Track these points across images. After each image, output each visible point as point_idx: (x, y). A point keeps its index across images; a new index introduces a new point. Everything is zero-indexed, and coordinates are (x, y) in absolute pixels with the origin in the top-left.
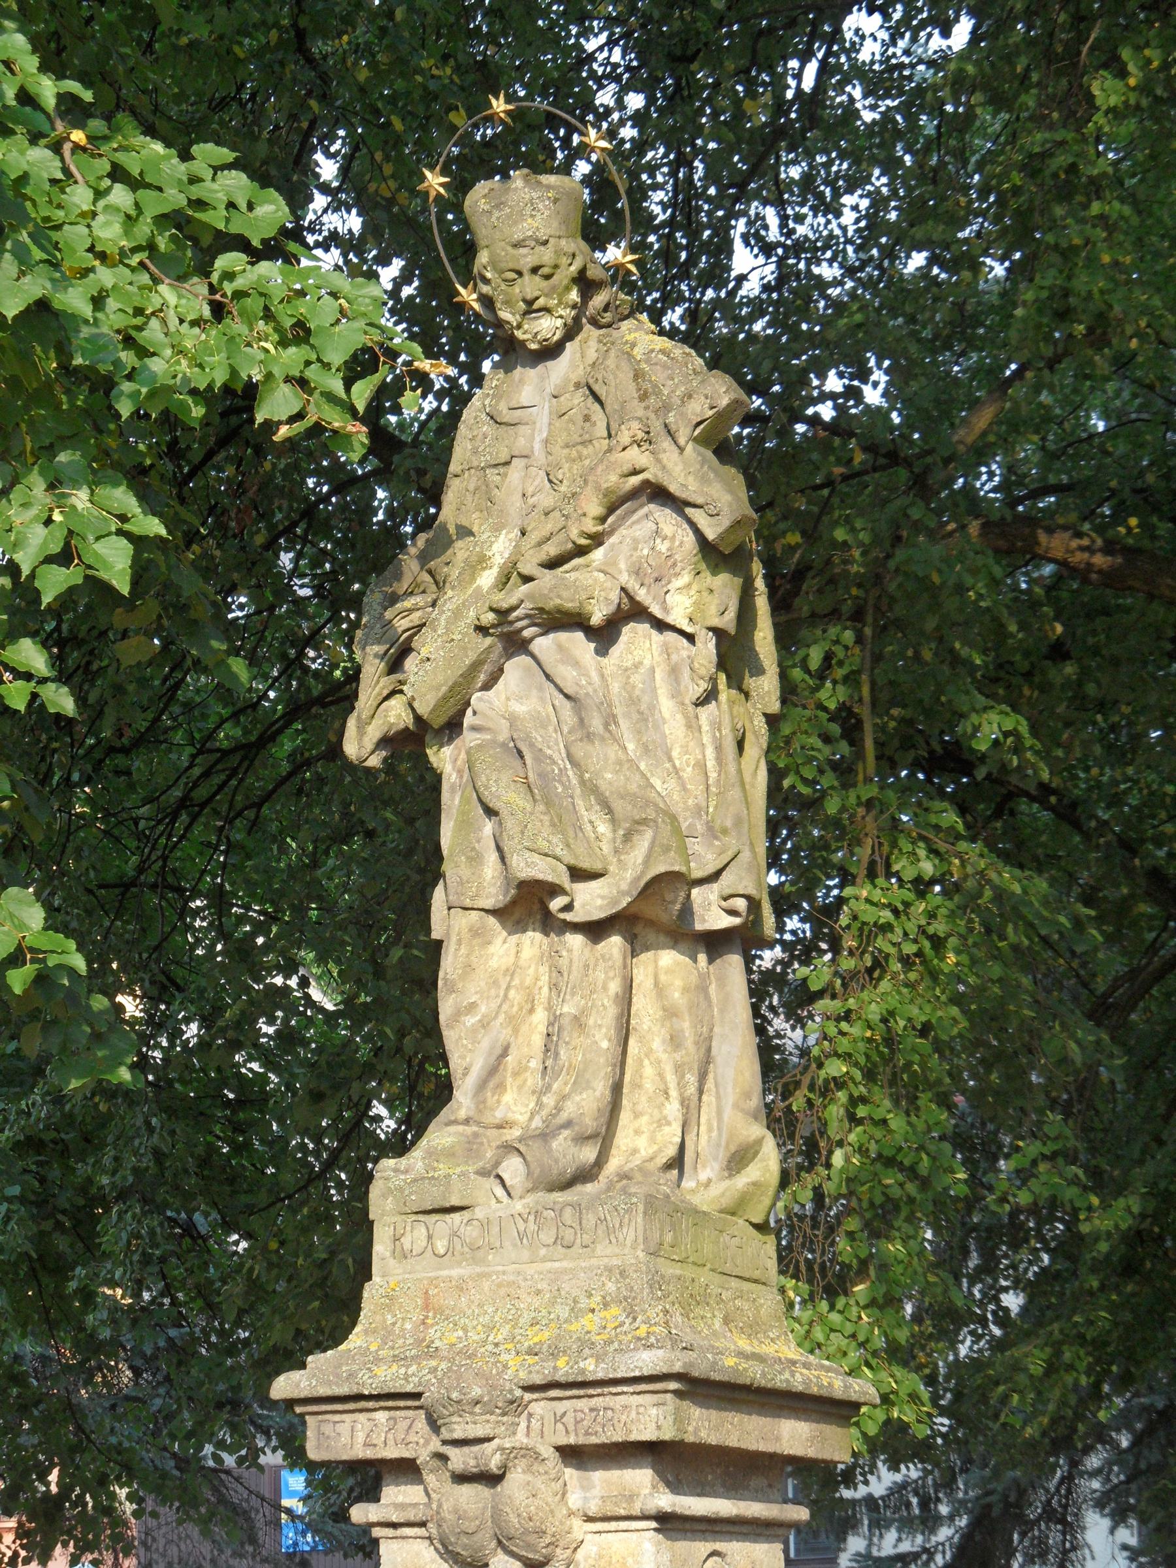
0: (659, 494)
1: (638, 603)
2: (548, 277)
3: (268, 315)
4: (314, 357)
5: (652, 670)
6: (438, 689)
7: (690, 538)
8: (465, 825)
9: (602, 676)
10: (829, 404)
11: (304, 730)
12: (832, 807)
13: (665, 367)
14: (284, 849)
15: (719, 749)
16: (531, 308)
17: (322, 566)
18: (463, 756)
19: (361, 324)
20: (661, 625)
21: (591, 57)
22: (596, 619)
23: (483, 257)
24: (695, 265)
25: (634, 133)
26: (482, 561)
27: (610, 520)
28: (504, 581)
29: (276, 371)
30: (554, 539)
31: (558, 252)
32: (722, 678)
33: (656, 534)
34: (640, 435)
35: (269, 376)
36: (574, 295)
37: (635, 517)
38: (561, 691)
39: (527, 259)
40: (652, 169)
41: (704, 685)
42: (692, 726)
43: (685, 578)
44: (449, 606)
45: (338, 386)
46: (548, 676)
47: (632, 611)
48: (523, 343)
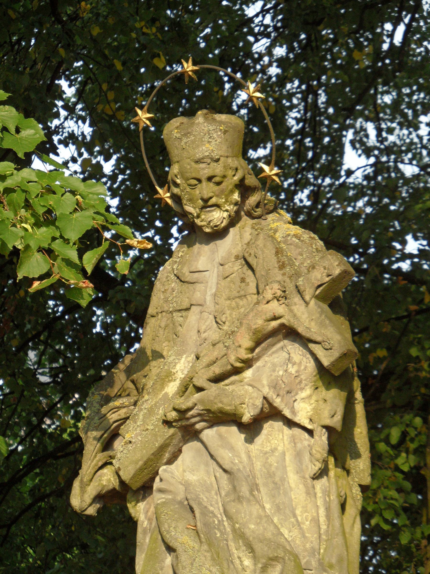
0: (290, 333)
1: (275, 408)
2: (218, 184)
3: (28, 205)
4: (58, 235)
5: (284, 454)
6: (136, 463)
7: (311, 364)
8: (152, 557)
9: (249, 457)
10: (408, 262)
11: (41, 473)
12: (404, 539)
13: (297, 246)
14: (25, 556)
15: (328, 509)
16: (206, 204)
17: (57, 361)
18: (152, 509)
19: (90, 213)
20: (290, 423)
21: (251, 20)
22: (246, 418)
23: (175, 169)
24: (318, 162)
25: (279, 71)
26: (168, 376)
27: (257, 350)
28: (184, 390)
29: (34, 245)
30: (219, 363)
31: (226, 167)
32: (332, 460)
33: (287, 362)
34: (279, 293)
35: (27, 247)
36: (236, 196)
37: (274, 349)
38: (221, 467)
39: (205, 171)
40: (290, 96)
41: (319, 465)
42: (310, 493)
43: (307, 392)
44: (145, 406)
45: (73, 255)
46: (212, 456)
47: (271, 413)
48: (200, 228)
